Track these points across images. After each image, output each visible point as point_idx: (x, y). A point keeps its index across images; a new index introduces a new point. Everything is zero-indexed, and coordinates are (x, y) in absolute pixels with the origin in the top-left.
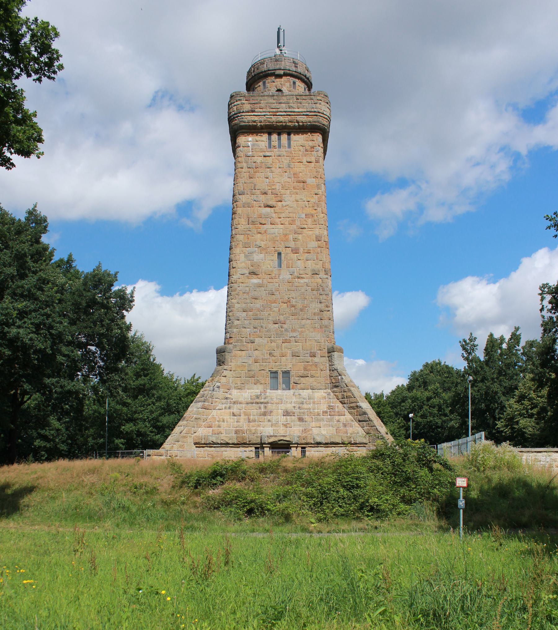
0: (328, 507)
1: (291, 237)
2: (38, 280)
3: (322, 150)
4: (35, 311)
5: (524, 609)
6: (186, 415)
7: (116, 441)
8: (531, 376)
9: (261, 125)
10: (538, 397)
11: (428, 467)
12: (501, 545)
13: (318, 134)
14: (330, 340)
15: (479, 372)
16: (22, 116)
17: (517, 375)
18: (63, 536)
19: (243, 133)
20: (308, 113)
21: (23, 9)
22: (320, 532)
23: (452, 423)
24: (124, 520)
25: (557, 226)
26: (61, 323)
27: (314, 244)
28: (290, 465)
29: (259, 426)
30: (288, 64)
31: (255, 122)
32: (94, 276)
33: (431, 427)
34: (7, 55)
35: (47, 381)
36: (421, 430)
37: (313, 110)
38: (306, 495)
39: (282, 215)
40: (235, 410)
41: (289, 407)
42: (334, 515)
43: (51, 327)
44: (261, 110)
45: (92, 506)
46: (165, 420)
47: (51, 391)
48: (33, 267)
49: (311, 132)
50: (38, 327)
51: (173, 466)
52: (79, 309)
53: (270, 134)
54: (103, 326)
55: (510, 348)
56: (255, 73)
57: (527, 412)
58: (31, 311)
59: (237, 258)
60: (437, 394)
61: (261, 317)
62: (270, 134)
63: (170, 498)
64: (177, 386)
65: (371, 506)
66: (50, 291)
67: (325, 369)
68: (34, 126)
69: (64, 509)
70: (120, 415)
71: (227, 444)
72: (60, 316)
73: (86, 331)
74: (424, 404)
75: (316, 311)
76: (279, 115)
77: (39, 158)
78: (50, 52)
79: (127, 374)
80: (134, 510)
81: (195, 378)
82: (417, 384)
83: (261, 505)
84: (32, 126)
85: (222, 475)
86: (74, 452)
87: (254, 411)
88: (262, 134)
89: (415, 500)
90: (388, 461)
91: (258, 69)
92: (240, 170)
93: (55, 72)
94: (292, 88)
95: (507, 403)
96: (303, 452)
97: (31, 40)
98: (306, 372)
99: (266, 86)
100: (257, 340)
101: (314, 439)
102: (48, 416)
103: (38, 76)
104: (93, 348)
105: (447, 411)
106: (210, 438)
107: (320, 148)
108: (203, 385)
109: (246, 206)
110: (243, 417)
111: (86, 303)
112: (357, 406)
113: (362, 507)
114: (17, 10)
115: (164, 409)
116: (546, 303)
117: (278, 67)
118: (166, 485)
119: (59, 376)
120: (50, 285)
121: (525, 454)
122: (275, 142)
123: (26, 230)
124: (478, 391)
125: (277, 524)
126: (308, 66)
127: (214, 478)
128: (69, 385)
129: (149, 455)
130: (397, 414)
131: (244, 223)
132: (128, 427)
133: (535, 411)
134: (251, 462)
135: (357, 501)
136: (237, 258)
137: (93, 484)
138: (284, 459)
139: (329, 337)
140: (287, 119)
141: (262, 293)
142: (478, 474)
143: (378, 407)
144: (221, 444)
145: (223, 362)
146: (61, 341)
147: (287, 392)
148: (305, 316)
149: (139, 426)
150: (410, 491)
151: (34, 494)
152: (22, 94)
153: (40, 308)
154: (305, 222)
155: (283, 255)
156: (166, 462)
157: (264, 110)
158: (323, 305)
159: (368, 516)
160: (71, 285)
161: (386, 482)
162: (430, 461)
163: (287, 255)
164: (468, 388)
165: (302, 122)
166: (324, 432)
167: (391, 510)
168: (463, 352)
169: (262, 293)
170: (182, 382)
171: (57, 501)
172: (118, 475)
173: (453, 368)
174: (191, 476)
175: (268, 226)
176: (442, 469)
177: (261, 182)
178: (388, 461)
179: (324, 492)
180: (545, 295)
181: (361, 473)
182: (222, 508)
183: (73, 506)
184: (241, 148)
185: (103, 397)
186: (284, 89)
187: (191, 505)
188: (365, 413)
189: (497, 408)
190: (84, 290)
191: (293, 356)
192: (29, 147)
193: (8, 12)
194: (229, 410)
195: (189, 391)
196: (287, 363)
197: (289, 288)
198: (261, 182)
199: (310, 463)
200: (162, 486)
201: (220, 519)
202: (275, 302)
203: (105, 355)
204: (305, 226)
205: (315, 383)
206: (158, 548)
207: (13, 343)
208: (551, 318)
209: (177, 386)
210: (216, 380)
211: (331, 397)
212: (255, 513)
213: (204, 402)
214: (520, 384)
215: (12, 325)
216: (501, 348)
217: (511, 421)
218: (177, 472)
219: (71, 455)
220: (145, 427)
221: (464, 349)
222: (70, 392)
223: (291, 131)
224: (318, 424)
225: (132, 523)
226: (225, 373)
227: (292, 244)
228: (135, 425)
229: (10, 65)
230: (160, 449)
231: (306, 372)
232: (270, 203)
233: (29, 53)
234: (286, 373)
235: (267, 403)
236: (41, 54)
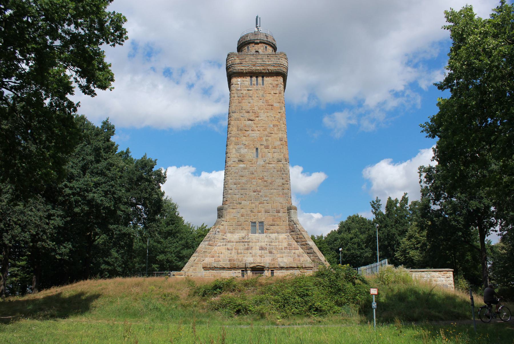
0: (288, 308)
1: (264, 139)
2: (107, 164)
4: (105, 183)
6: (198, 249)
8: (416, 223)
11: (352, 282)
12: (401, 332)
15: (383, 221)
17: (407, 223)
18: (117, 327)
19: (235, 76)
21: (107, 7)
22: (283, 325)
23: (367, 254)
24: (157, 317)
26: (121, 191)
27: (279, 143)
28: (264, 282)
29: (244, 256)
32: (142, 162)
33: (353, 256)
34: (96, 32)
35: (111, 227)
36: (347, 258)
40: (229, 246)
41: (263, 244)
42: (293, 313)
43: (114, 193)
46: (185, 252)
47: (113, 233)
49: (276, 76)
50: (106, 193)
51: (189, 282)
52: (132, 182)
53: (251, 77)
54: (146, 193)
55: (402, 206)
57: (414, 246)
60: (356, 236)
62: (251, 77)
63: (187, 302)
66: (114, 171)
68: (109, 72)
69: (118, 310)
70: (156, 249)
71: (223, 268)
72: (120, 186)
73: (136, 196)
77: (111, 90)
79: (161, 223)
82: (344, 229)
84: (108, 72)
85: (220, 288)
86: (126, 272)
87: (241, 247)
89: (344, 304)
90: (326, 279)
93: (123, 41)
96: (272, 273)
97: (110, 24)
100: (243, 202)
102: (111, 249)
103: (113, 43)
104: (140, 207)
105: (363, 246)
108: (209, 230)
110: (234, 251)
112: (306, 244)
113: (310, 308)
115: (184, 245)
116: (423, 177)
117: (256, 38)
118: (184, 294)
119: (119, 224)
120: (115, 167)
121: (414, 273)
124: (383, 233)
125: (256, 320)
126: (274, 37)
127: (215, 290)
128: (124, 230)
129: (174, 275)
130: (331, 249)
132: (161, 257)
133: (419, 246)
134: (239, 279)
136: (231, 151)
137: (138, 293)
138: (260, 278)
140: (261, 68)
141: (246, 173)
143: (320, 244)
144: (220, 268)
146: (120, 202)
148: (273, 188)
149: (168, 256)
150: (341, 297)
151: (99, 299)
153: (108, 181)
155: (259, 150)
156: (185, 279)
158: (284, 180)
159: (314, 314)
160: (127, 167)
161: (325, 292)
162: (353, 278)
166: (285, 260)
167: (329, 310)
168: (373, 209)
169: (246, 173)
170: (196, 229)
172: (154, 287)
173: (366, 219)
174: (200, 288)
176: (361, 283)
177: (246, 105)
179: (286, 299)
181: (309, 286)
182: (220, 309)
184: (234, 85)
185: (145, 238)
186: (260, 51)
188: (311, 248)
189: (395, 244)
190: (136, 170)
192: (105, 84)
193: (98, 8)
194: (225, 247)
196: (262, 217)
199: (277, 280)
200: (181, 294)
201: (219, 316)
203: (148, 211)
204: (273, 132)
205: (279, 229)
206: (178, 335)
208: (427, 187)
209: (193, 231)
210: (217, 227)
212: (241, 313)
214: (409, 229)
216: (396, 206)
217: (404, 252)
219: (124, 274)
220: (172, 257)
221: (373, 207)
222: (125, 234)
224: (281, 255)
226: (223, 223)
227: (265, 143)
228: (165, 255)
229: (98, 37)
232: (251, 118)
234: (262, 223)
235: (249, 242)
236: (115, 31)
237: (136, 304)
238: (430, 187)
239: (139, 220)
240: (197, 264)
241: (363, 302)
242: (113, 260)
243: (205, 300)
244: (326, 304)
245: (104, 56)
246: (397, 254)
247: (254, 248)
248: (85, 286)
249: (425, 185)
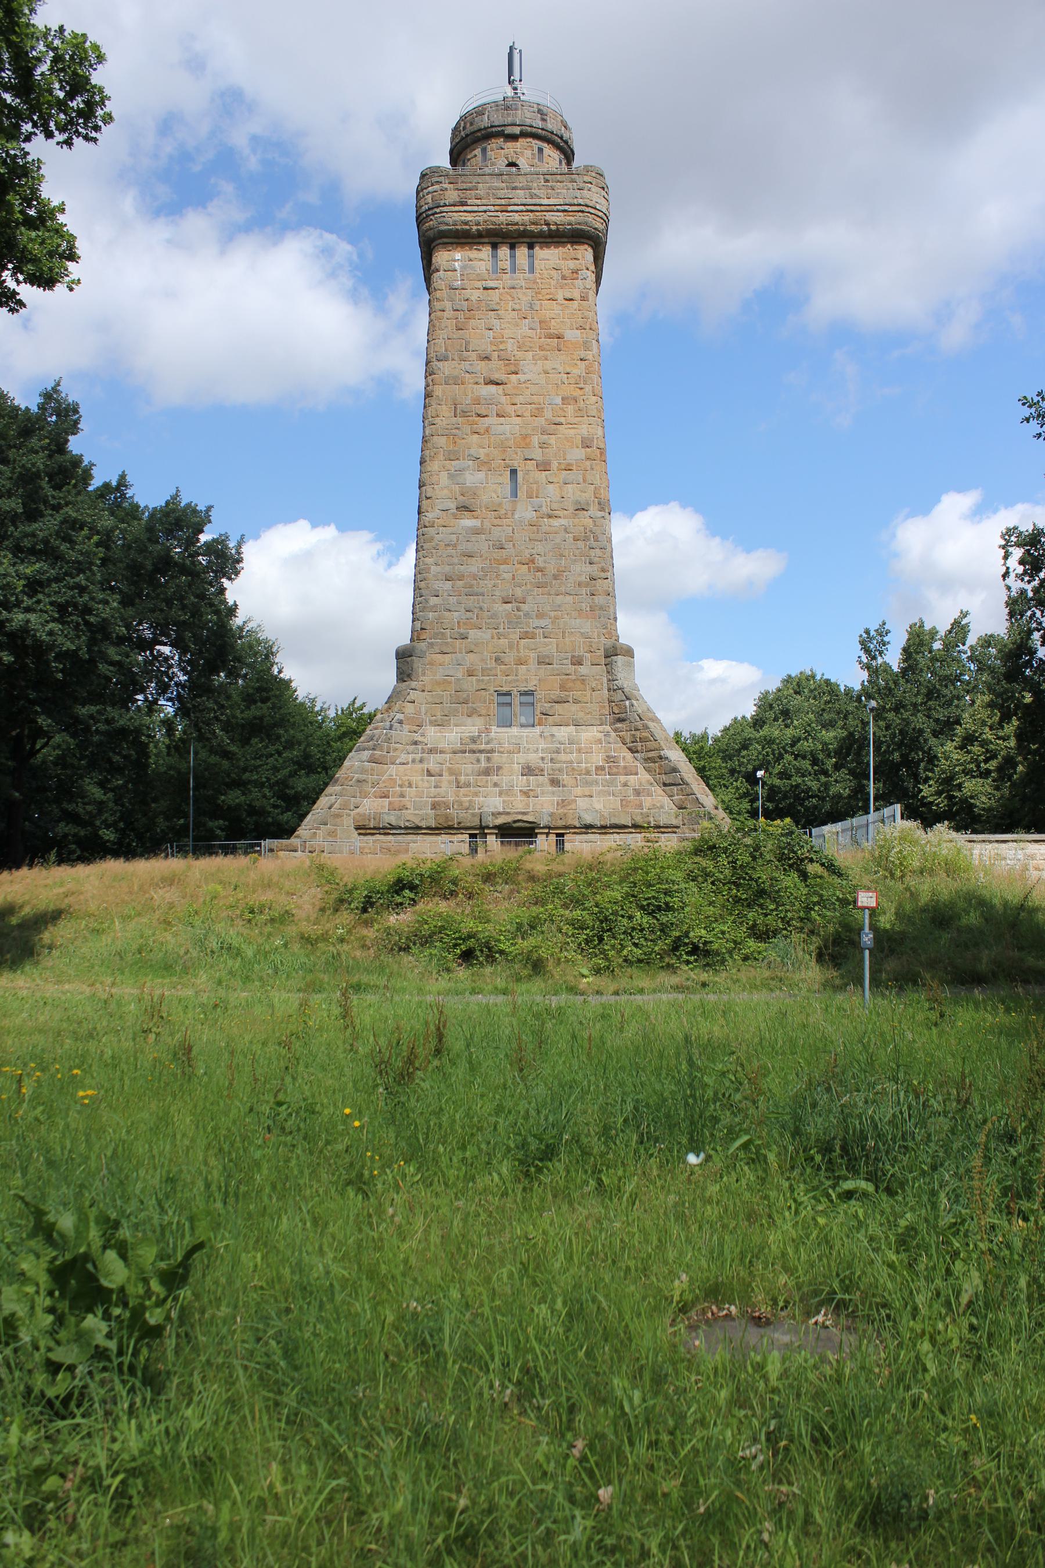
0: (613, 947)
2: (62, 523)
3: (593, 277)
4: (57, 580)
5: (1010, 1138)
6: (340, 774)
7: (210, 824)
8: (987, 698)
10: (999, 738)
11: (798, 870)
12: (942, 1016)
14: (610, 633)
16: (39, 212)
25: (1044, 417)
26: (107, 602)
27: (579, 453)
28: (540, 868)
29: (476, 794)
31: (466, 223)
33: (797, 798)
34: (8, 97)
38: (572, 923)
39: (519, 400)
41: (533, 758)
42: (625, 961)
43: (87, 610)
44: (478, 202)
45: (170, 947)
47: (87, 729)
48: (54, 497)
49: (573, 243)
53: (495, 246)
55: (948, 646)
56: (468, 131)
57: (978, 766)
58: (49, 580)
59: (434, 479)
61: (480, 590)
62: (495, 246)
63: (318, 930)
64: (323, 721)
65: (693, 943)
66: (87, 543)
71: (416, 829)
74: (786, 752)
75: (583, 578)
78: (88, 91)
79: (229, 697)
80: (250, 953)
83: (487, 942)
84: (57, 231)
85: (413, 888)
86: (129, 844)
87: (467, 766)
89: (775, 933)
90: (723, 860)
91: (472, 124)
92: (439, 313)
93: (97, 129)
95: (940, 749)
96: (560, 844)
98: (563, 694)
100: (473, 633)
102: (81, 777)
103: (65, 136)
104: (166, 650)
107: (589, 273)
110: (446, 777)
111: (153, 564)
112: (660, 757)
113: (675, 948)
114: (27, 11)
115: (298, 763)
116: (1013, 563)
117: (510, 120)
118: (307, 906)
120: (85, 532)
121: (978, 846)
123: (39, 429)
124: (888, 728)
127: (397, 893)
130: (732, 772)
131: (447, 414)
132: (233, 797)
133: (993, 765)
134: (467, 862)
135: (668, 936)
136: (434, 479)
137: (171, 906)
140: (527, 217)
141: (481, 545)
142: (892, 883)
143: (699, 759)
144: (406, 828)
145: (409, 676)
146: (107, 637)
148: (563, 589)
149: (254, 795)
150: (766, 915)
151: (62, 923)
152: (39, 168)
153: (66, 574)
154: (561, 413)
155: (520, 474)
157: (484, 201)
158: (595, 567)
159: (688, 962)
162: (802, 860)
164: (868, 723)
166: (598, 806)
167: (730, 952)
168: (862, 654)
170: (332, 714)
171: (104, 938)
172: (219, 888)
175: (492, 420)
176: (826, 874)
177: (480, 338)
178: (723, 860)
179: (606, 919)
180: (1011, 549)
181: (673, 882)
182: (414, 950)
183: (135, 947)
186: (522, 162)
187: (356, 944)
188: (675, 770)
189: (922, 760)
190: (149, 540)
191: (539, 663)
192: (51, 269)
193: (12, 12)
194: (420, 766)
195: (343, 729)
196: (530, 676)
197: (533, 536)
200: (300, 907)
204: (562, 420)
205: (581, 714)
207: (18, 641)
210: (396, 708)
214: (966, 715)
215: (15, 606)
217: (948, 783)
218: (329, 882)
219: (125, 851)
220: (262, 798)
222: (123, 732)
225: (247, 977)
226: (413, 695)
227: (537, 454)
231: (563, 694)
232: (496, 376)
233: (50, 91)
235: (492, 751)
236: (71, 95)
237: (169, 937)
238: (1036, 591)
239: (163, 688)
241: (831, 928)
242: (89, 808)
243: (368, 924)
244: (723, 932)
245: (40, 179)
246: (927, 791)
248: (16, 887)
249: (1020, 584)
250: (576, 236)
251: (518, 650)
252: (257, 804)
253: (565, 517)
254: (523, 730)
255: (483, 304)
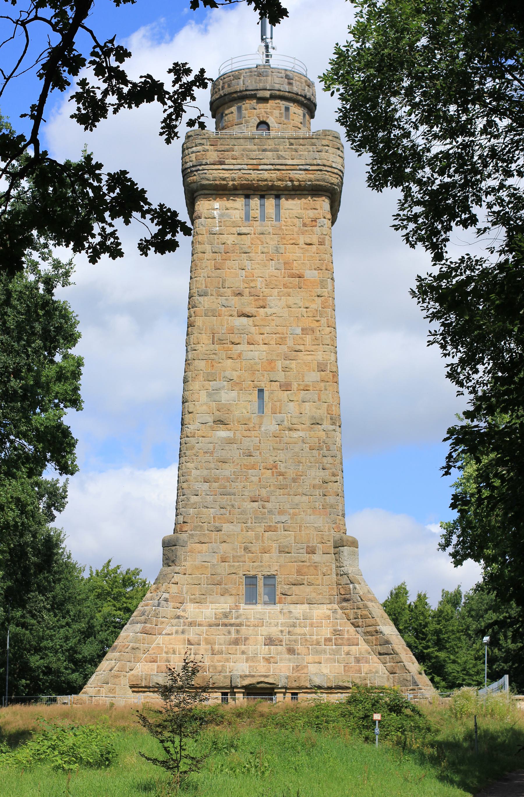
9: (233, 185)
13: (324, 198)
14: (338, 527)
19: (207, 196)
20: (307, 167)
29: (227, 660)
30: (277, 80)
31: (224, 179)
37: (315, 162)
39: (267, 329)
40: (192, 634)
41: (274, 631)
44: (234, 161)
53: (247, 197)
59: (195, 397)
67: (329, 572)
75: (317, 482)
76: (262, 170)
81: (110, 568)
87: (220, 637)
88: (236, 198)
92: (200, 255)
94: (283, 119)
99: (243, 115)
100: (226, 527)
101: (310, 680)
106: (155, 678)
107: (326, 221)
109: (210, 314)
117: (261, 85)
122: (256, 213)
131: (206, 342)
136: (195, 397)
139: (335, 523)
140: (274, 175)
141: (233, 452)
145: (173, 561)
147: (270, 608)
148: (300, 490)
155: (266, 394)
157: (239, 161)
158: (327, 472)
163: (273, 393)
165: (299, 181)
169: (233, 452)
184: (203, 219)
186: (271, 121)
188: (387, 642)
191: (280, 552)
194: (182, 636)
196: (271, 562)
197: (276, 446)
198: (234, 276)
202: (253, 467)
204: (301, 347)
205: (314, 595)
210: (163, 588)
211: (338, 617)
213: (145, 623)
220: (58, 662)
223: (280, 192)
224: (317, 658)
227: (281, 376)
230: (80, 694)
232: (248, 310)
235: (240, 625)
240: (117, 677)
247: (250, 641)
250: (314, 190)
251: (263, 541)
252: (54, 666)
253: (303, 430)
254: (266, 607)
255: (237, 247)
